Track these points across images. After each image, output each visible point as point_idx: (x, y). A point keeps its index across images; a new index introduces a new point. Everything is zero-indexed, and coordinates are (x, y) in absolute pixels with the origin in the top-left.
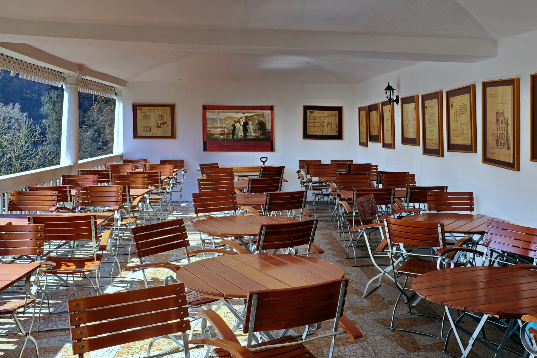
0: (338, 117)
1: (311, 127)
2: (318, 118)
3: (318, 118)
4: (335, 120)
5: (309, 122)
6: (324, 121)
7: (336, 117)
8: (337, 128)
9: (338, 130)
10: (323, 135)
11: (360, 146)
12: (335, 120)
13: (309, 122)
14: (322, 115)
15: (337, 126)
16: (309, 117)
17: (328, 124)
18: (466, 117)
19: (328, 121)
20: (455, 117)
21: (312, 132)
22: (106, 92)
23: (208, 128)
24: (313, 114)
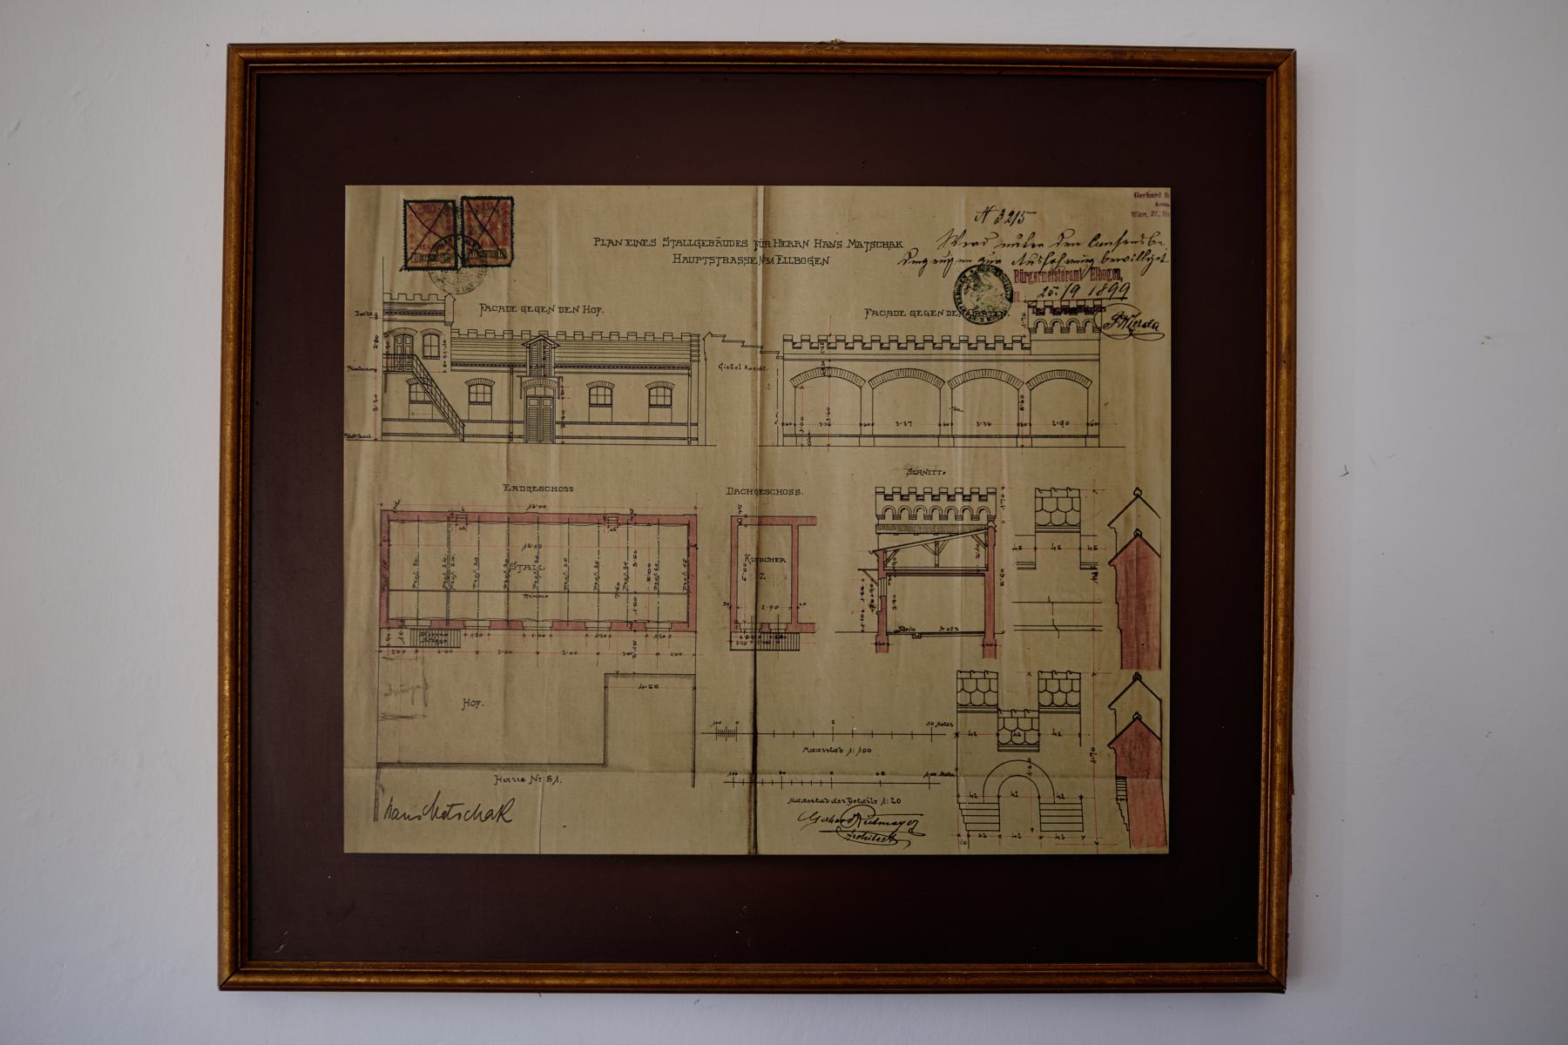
0: (1157, 355)
1: (439, 634)
2: (630, 392)
3: (630, 392)
4: (1091, 433)
5: (390, 518)
6: (788, 463)
7: (1119, 351)
8: (1133, 655)
9: (1158, 718)
10: (754, 861)
11: (1287, 991)
12: (1091, 433)
13: (390, 518)
14: (378, 327)
15: (1131, 600)
16: (400, 360)
17: (888, 568)
18: (246, 443)
19: (884, 466)
20: (466, 439)
21: (471, 788)
22: (1281, 774)
23: (1166, 205)
24: (495, 284)
